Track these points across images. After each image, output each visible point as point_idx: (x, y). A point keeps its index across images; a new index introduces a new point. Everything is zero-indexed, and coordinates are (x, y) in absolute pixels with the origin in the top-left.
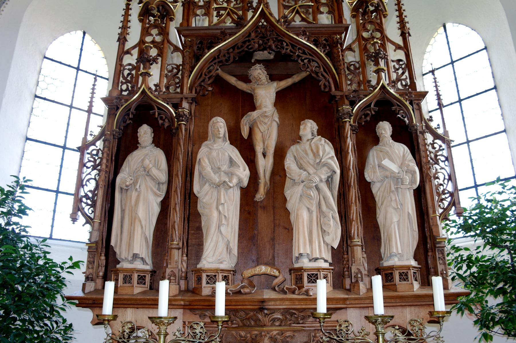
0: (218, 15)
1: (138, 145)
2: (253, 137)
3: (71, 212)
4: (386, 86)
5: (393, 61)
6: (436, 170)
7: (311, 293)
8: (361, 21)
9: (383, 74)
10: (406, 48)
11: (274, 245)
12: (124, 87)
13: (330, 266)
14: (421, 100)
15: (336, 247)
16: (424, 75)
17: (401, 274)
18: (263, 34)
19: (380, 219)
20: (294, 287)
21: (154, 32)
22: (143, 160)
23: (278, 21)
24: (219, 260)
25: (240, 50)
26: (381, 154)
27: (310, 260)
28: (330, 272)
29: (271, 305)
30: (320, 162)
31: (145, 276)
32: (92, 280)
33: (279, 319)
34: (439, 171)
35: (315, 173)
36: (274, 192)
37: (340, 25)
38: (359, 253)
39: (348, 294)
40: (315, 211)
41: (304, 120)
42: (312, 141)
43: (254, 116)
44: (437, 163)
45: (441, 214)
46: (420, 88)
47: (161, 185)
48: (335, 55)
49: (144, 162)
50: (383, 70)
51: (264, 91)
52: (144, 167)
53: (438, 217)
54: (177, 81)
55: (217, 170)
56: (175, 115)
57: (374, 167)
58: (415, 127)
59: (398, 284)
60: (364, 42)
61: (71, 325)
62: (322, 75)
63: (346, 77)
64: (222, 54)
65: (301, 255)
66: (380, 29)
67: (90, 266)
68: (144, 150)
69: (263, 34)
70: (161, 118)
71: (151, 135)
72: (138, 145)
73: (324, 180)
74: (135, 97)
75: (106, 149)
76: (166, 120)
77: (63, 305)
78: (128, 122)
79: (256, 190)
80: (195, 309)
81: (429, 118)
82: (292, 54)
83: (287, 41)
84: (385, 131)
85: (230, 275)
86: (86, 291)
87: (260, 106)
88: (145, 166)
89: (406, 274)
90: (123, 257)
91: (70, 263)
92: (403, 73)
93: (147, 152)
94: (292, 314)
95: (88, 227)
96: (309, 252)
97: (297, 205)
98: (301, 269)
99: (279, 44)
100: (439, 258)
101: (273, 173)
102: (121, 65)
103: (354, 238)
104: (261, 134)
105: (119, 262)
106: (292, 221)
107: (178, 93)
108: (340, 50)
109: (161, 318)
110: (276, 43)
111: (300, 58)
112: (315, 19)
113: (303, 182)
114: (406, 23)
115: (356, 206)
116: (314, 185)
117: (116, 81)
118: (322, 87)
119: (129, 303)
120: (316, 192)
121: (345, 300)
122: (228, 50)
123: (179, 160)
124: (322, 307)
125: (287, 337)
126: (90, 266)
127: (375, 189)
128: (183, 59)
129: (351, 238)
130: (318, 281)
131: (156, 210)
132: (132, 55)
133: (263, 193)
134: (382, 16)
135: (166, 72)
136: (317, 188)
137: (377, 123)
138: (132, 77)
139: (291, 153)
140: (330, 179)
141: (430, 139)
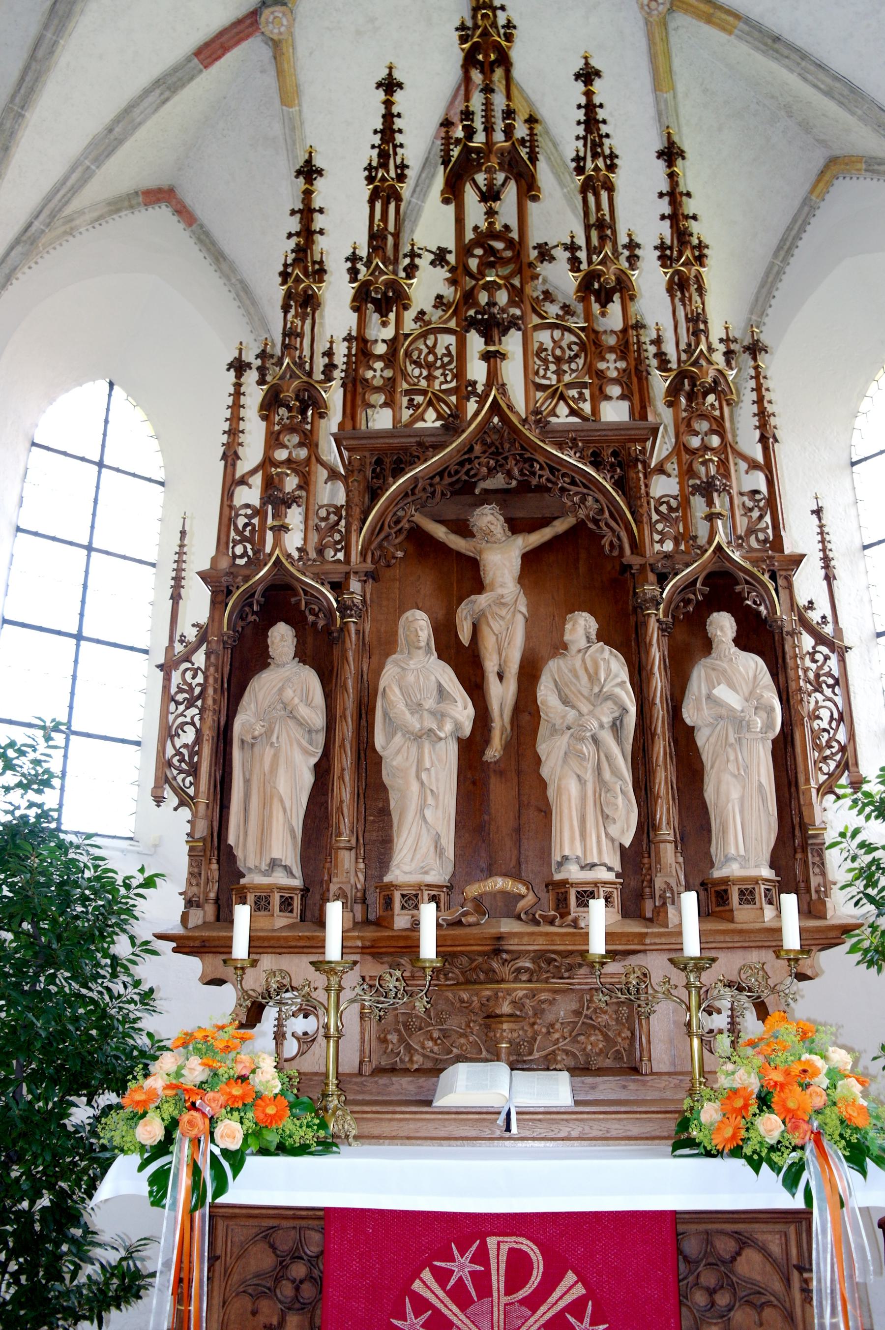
0: (411, 404)
2: (480, 643)
6: (817, 702)
7: (582, 925)
8: (684, 414)
9: (719, 522)
10: (768, 468)
11: (519, 840)
12: (239, 550)
15: (627, 844)
16: (853, 464)
18: (497, 448)
19: (709, 794)
20: (553, 913)
22: (281, 690)
23: (525, 421)
25: (454, 479)
26: (713, 675)
27: (582, 868)
29: (512, 945)
30: (600, 691)
31: (292, 898)
32: (198, 906)
33: (527, 970)
35: (591, 713)
36: (519, 744)
37: (642, 423)
38: (669, 855)
39: (647, 927)
41: (572, 611)
44: (818, 689)
47: (314, 734)
48: (632, 485)
49: (284, 694)
50: (719, 515)
51: (499, 556)
52: (283, 703)
53: (814, 792)
54: (337, 537)
55: (416, 708)
57: (698, 700)
61: (152, 990)
62: (607, 525)
63: (652, 526)
65: (565, 858)
67: (194, 882)
68: (282, 670)
69: (497, 448)
73: (606, 726)
75: (212, 669)
76: (321, 615)
77: (133, 954)
78: (252, 618)
79: (487, 741)
80: (381, 953)
82: (550, 485)
84: (722, 630)
85: (442, 894)
86: (191, 925)
87: (492, 583)
88: (285, 700)
90: (251, 863)
91: (140, 879)
92: (761, 517)
93: (287, 674)
94: (550, 961)
95: (185, 813)
96: (579, 853)
97: (558, 769)
98: (564, 883)
99: (527, 466)
100: (814, 863)
101: (517, 709)
102: (231, 507)
103: (660, 829)
105: (243, 876)
106: (550, 799)
107: (339, 561)
109: (330, 962)
110: (521, 465)
112: (595, 410)
113: (569, 728)
114: (769, 416)
115: (666, 771)
116: (588, 734)
117: (223, 539)
118: (607, 547)
119: (266, 944)
120: (592, 748)
121: (644, 935)
122: (432, 478)
124: (598, 946)
125: (543, 1002)
126: (194, 882)
127: (701, 739)
128: (347, 496)
129: (656, 828)
130: (591, 901)
131: (308, 779)
132: (250, 487)
133: (499, 747)
134: (724, 404)
135: (317, 521)
136: (595, 740)
138: (253, 531)
140: (618, 723)
141: (807, 642)
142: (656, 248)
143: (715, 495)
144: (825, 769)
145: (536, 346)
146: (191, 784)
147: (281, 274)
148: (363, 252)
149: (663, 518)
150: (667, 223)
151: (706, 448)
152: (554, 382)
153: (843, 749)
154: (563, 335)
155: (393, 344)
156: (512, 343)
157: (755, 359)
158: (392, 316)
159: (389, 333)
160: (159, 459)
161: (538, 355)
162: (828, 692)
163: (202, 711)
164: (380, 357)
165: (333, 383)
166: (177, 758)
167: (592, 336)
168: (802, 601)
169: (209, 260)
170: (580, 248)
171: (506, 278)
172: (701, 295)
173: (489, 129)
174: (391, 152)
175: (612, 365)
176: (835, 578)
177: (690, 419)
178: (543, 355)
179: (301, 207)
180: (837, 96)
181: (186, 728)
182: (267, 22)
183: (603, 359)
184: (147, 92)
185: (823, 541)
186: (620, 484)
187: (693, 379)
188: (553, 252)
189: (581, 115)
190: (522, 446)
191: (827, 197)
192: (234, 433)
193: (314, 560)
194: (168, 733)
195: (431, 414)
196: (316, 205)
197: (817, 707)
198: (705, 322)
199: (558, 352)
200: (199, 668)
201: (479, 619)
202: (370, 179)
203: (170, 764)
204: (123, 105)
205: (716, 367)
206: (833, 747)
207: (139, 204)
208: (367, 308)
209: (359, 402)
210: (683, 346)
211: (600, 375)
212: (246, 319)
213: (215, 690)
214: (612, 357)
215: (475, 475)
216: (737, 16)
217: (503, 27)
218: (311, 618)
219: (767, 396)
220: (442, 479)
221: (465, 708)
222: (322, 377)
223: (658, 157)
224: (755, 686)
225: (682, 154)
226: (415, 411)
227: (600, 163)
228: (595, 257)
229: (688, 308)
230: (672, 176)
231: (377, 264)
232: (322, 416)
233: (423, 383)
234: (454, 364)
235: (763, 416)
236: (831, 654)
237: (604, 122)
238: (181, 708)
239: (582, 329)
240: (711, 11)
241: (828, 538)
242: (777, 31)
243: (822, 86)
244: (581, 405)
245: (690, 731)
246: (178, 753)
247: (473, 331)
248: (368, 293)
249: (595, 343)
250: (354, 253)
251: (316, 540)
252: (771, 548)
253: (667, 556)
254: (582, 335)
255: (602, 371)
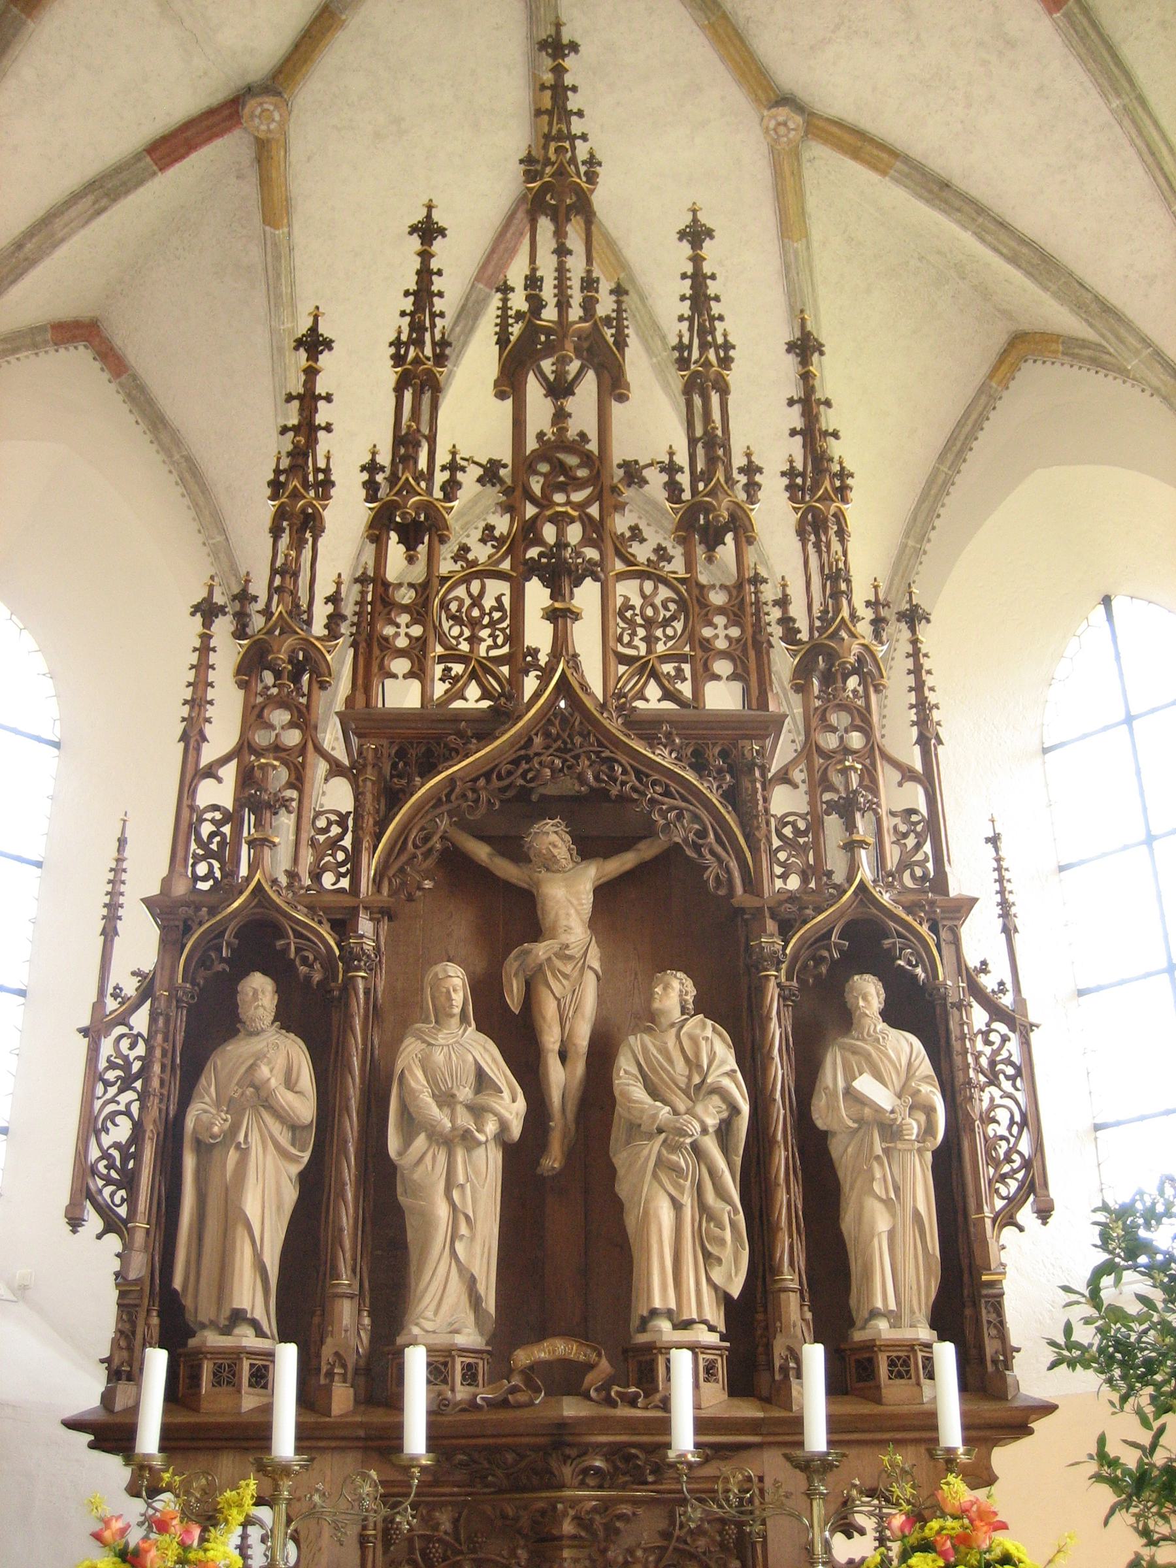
1: (238, 1026)
3: (67, 1202)
4: (870, 885)
5: (893, 814)
6: (992, 1099)
8: (818, 703)
9: (863, 852)
10: (928, 779)
12: (202, 869)
13: (722, 1340)
14: (959, 919)
16: (1045, 751)
17: (892, 1360)
18: (565, 742)
20: (633, 1389)
21: (280, 717)
23: (603, 707)
24: (451, 1324)
25: (506, 782)
26: (853, 1059)
27: (676, 1327)
28: (721, 1356)
30: (703, 1081)
33: (598, 1470)
34: (998, 1101)
40: (689, 1205)
41: (663, 970)
42: (682, 1027)
43: (537, 955)
44: (993, 1081)
45: (997, 1215)
46: (957, 886)
50: (862, 844)
53: (988, 1222)
55: (446, 1099)
56: (337, 953)
58: (942, 990)
59: (886, 1386)
60: (821, 761)
62: (713, 852)
64: (457, 790)
65: (654, 1313)
66: (863, 722)
69: (565, 742)
70: (305, 961)
71: (273, 999)
72: (238, 1026)
73: (711, 1130)
74: (236, 905)
76: (317, 966)
78: (220, 967)
81: (978, 965)
82: (635, 796)
83: (623, 762)
84: (865, 999)
88: (257, 1082)
89: (904, 1361)
90: (203, 1317)
92: (918, 846)
95: (113, 1242)
99: (604, 768)
100: (989, 1322)
102: (192, 808)
104: (556, 1003)
105: (192, 1334)
107: (342, 890)
108: (758, 785)
111: (658, 807)
113: (660, 1131)
114: (931, 709)
116: (689, 1140)
118: (711, 883)
120: (691, 1160)
122: (475, 780)
123: (351, 1072)
127: (836, 1148)
128: (356, 799)
129: (775, 1270)
132: (220, 780)
134: (871, 689)
135: (313, 833)
136: (696, 1148)
137: (848, 977)
138: (223, 844)
139: (630, 1055)
141: (979, 1016)
142: (783, 474)
143: (858, 815)
144: (1004, 1191)
145: (619, 601)
146: (123, 1200)
147: (270, 484)
148: (384, 459)
149: (787, 843)
150: (799, 439)
151: (846, 751)
152: (643, 652)
153: (1027, 1164)
154: (656, 588)
155: (423, 589)
156: (587, 595)
157: (913, 630)
158: (422, 549)
159: (418, 573)
160: (52, 709)
161: (621, 614)
162: (1007, 1085)
163: (142, 1097)
164: (405, 609)
165: (341, 640)
166: (105, 1162)
167: (696, 592)
168: (972, 961)
169: (143, 426)
170: (681, 470)
171: (582, 506)
172: (842, 541)
173: (563, 305)
174: (428, 325)
175: (720, 633)
176: (1016, 930)
177: (825, 710)
178: (629, 614)
179: (301, 391)
180: (1024, 265)
181: (120, 1119)
182: (252, 116)
183: (710, 624)
184: (75, 198)
185: (1000, 880)
186: (731, 796)
187: (831, 656)
188: (646, 473)
189: (686, 287)
190: (598, 740)
191: (1012, 384)
192: (198, 703)
193: (308, 888)
194: (91, 1126)
195: (473, 691)
196: (320, 389)
197: (993, 1106)
198: (848, 581)
199: (649, 612)
200: (139, 1035)
201: (532, 976)
202: (398, 359)
203: (94, 1171)
204: (40, 213)
205: (862, 641)
206: (1013, 1161)
207: (46, 342)
208: (389, 538)
209: (375, 669)
210: (816, 613)
211: (706, 645)
212: (193, 513)
213: (163, 1067)
214: (720, 620)
215: (532, 780)
216: (894, 153)
217: (584, 163)
218: (303, 969)
219: (929, 681)
220: (488, 781)
221: (514, 1101)
222: (326, 632)
223: (788, 351)
224: (908, 1078)
225: (819, 349)
226: (453, 685)
227: (711, 355)
228: (701, 486)
229: (825, 555)
230: (806, 377)
231: (407, 479)
232: (323, 686)
233: (465, 647)
234: (507, 622)
235: (923, 707)
236: (1011, 1035)
237: (717, 299)
238: (112, 1091)
239: (683, 581)
240: (859, 144)
241: (1007, 875)
242: (944, 174)
243: (1005, 251)
244: (679, 686)
245: (823, 1137)
246: (105, 1155)
247: (535, 580)
248: (391, 518)
249: (698, 601)
250: (373, 460)
251: (310, 859)
252: (932, 889)
253: (792, 898)
254: (683, 589)
255: (708, 640)
